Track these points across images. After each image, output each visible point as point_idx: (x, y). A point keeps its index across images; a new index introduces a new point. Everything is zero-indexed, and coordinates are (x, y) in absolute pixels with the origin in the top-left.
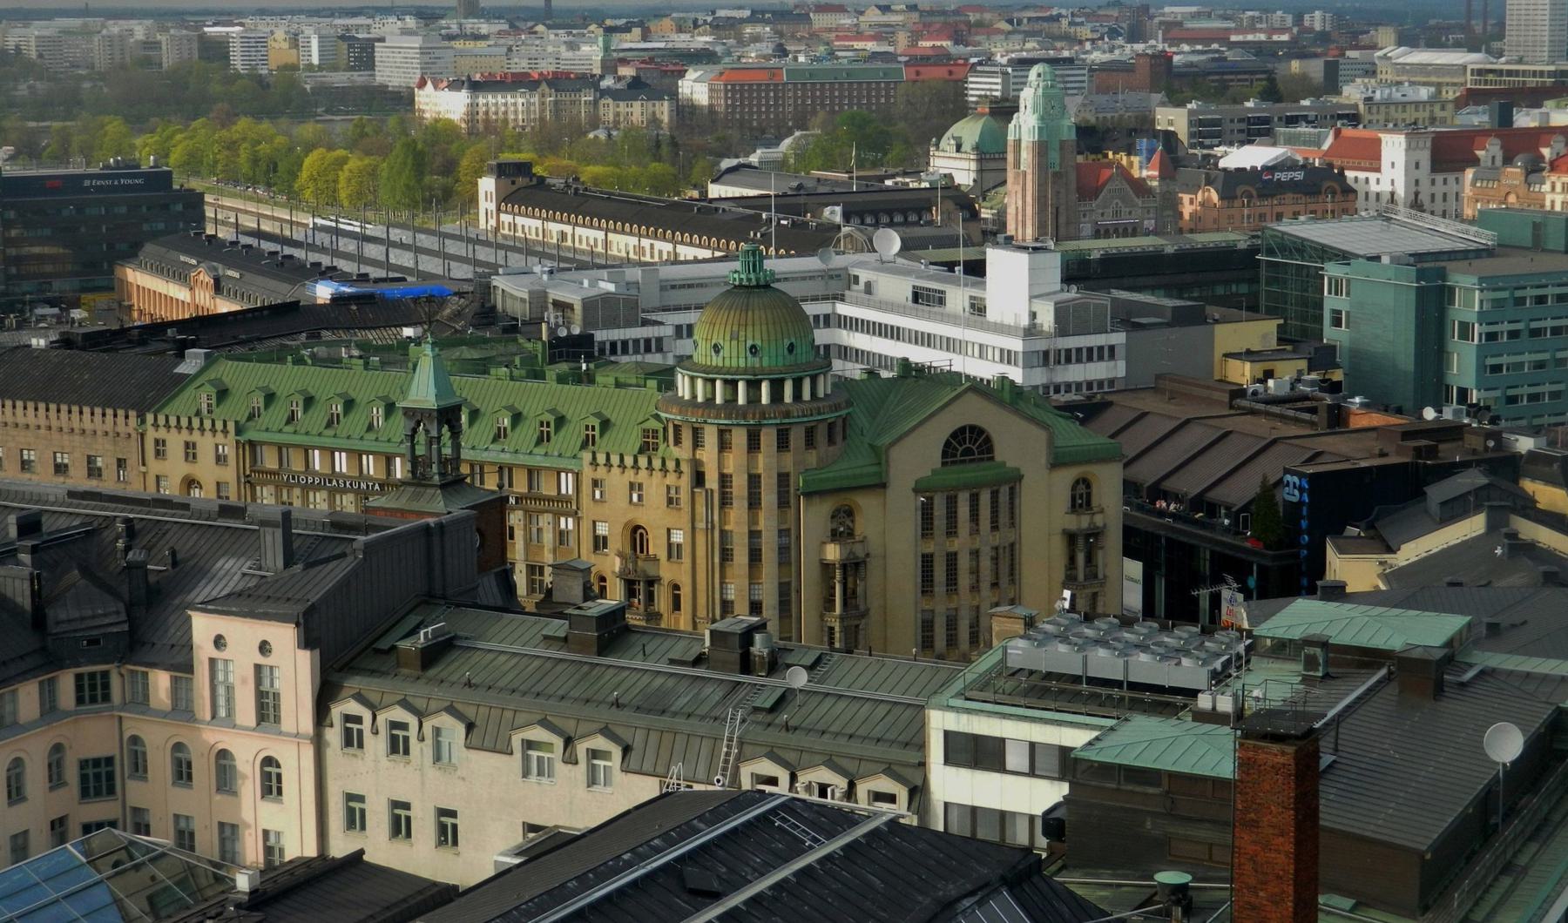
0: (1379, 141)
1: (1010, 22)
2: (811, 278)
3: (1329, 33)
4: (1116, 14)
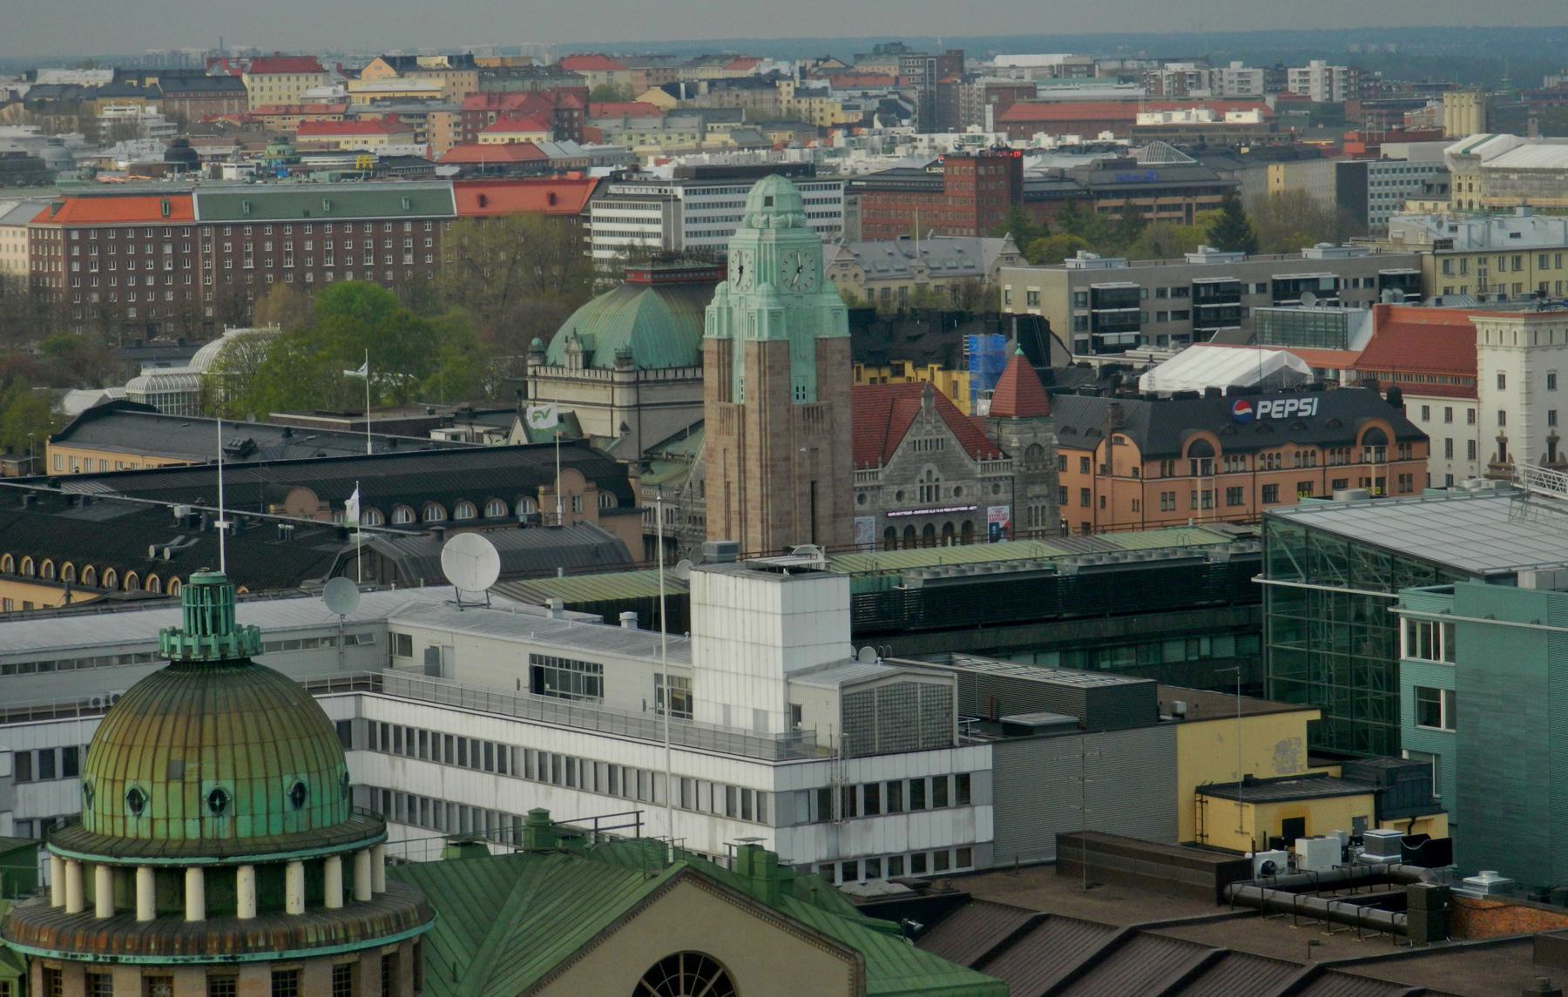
0: (1471, 332)
1: (672, 89)
2: (309, 643)
3: (1341, 106)
4: (894, 72)
